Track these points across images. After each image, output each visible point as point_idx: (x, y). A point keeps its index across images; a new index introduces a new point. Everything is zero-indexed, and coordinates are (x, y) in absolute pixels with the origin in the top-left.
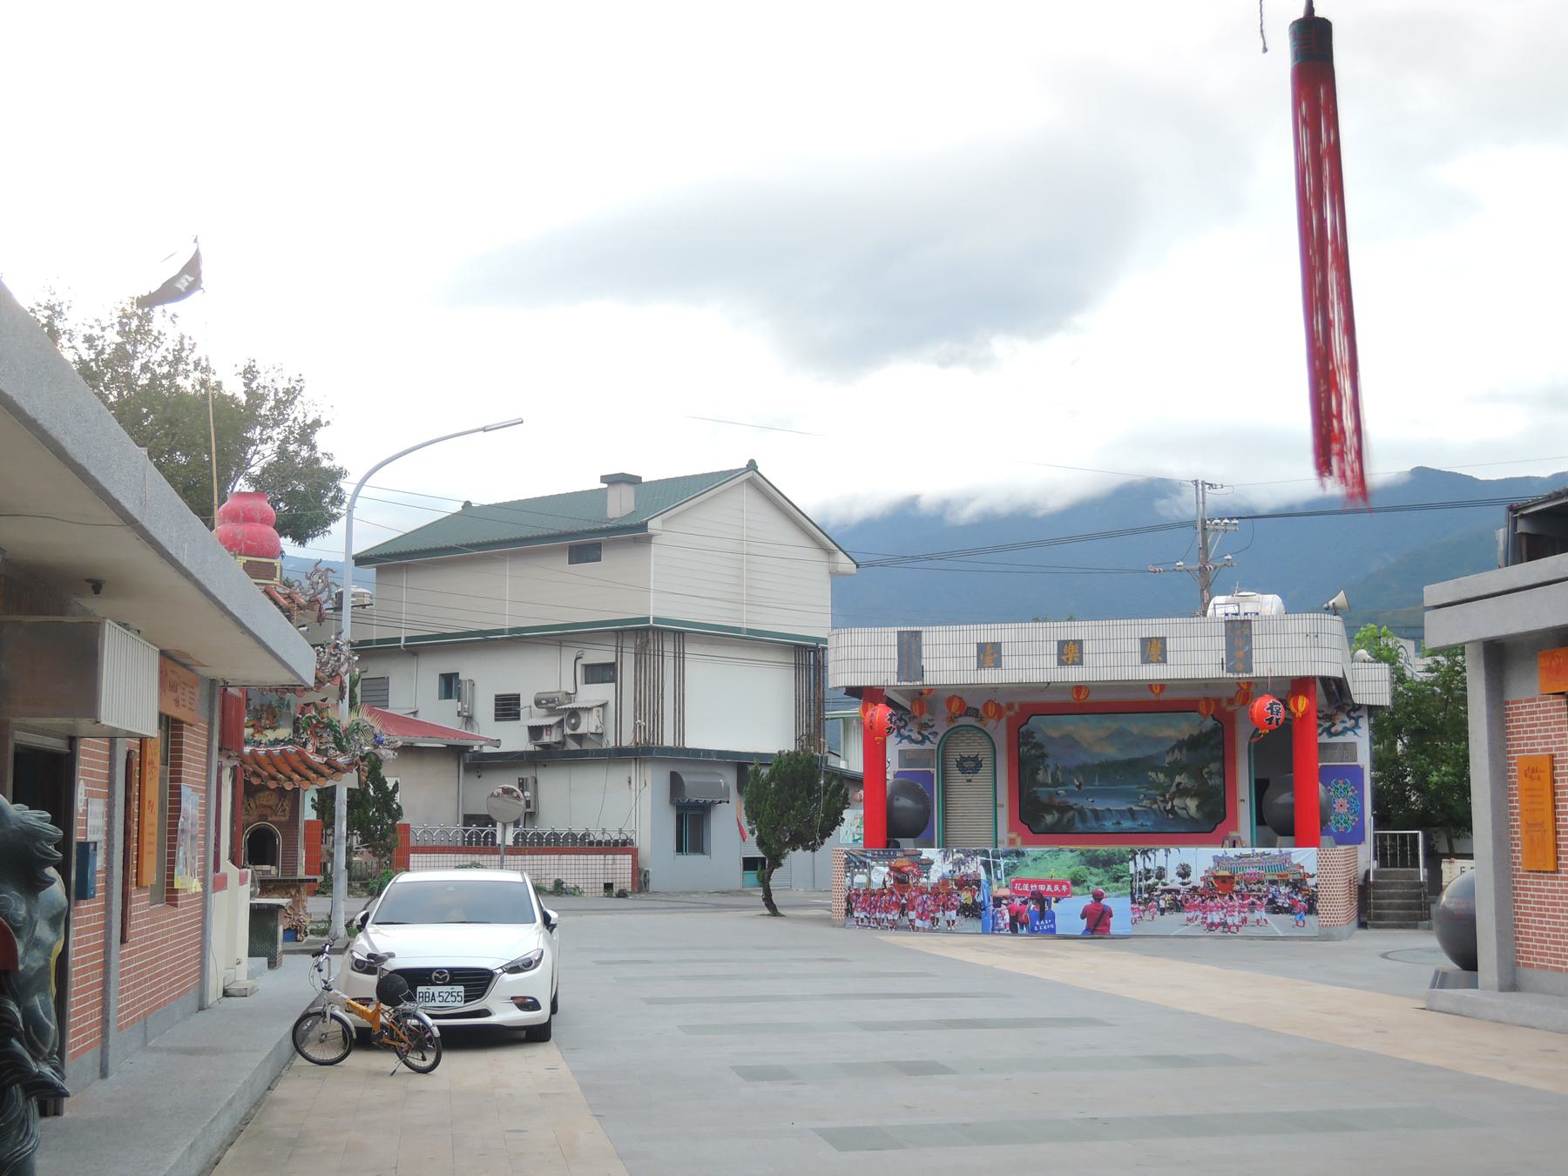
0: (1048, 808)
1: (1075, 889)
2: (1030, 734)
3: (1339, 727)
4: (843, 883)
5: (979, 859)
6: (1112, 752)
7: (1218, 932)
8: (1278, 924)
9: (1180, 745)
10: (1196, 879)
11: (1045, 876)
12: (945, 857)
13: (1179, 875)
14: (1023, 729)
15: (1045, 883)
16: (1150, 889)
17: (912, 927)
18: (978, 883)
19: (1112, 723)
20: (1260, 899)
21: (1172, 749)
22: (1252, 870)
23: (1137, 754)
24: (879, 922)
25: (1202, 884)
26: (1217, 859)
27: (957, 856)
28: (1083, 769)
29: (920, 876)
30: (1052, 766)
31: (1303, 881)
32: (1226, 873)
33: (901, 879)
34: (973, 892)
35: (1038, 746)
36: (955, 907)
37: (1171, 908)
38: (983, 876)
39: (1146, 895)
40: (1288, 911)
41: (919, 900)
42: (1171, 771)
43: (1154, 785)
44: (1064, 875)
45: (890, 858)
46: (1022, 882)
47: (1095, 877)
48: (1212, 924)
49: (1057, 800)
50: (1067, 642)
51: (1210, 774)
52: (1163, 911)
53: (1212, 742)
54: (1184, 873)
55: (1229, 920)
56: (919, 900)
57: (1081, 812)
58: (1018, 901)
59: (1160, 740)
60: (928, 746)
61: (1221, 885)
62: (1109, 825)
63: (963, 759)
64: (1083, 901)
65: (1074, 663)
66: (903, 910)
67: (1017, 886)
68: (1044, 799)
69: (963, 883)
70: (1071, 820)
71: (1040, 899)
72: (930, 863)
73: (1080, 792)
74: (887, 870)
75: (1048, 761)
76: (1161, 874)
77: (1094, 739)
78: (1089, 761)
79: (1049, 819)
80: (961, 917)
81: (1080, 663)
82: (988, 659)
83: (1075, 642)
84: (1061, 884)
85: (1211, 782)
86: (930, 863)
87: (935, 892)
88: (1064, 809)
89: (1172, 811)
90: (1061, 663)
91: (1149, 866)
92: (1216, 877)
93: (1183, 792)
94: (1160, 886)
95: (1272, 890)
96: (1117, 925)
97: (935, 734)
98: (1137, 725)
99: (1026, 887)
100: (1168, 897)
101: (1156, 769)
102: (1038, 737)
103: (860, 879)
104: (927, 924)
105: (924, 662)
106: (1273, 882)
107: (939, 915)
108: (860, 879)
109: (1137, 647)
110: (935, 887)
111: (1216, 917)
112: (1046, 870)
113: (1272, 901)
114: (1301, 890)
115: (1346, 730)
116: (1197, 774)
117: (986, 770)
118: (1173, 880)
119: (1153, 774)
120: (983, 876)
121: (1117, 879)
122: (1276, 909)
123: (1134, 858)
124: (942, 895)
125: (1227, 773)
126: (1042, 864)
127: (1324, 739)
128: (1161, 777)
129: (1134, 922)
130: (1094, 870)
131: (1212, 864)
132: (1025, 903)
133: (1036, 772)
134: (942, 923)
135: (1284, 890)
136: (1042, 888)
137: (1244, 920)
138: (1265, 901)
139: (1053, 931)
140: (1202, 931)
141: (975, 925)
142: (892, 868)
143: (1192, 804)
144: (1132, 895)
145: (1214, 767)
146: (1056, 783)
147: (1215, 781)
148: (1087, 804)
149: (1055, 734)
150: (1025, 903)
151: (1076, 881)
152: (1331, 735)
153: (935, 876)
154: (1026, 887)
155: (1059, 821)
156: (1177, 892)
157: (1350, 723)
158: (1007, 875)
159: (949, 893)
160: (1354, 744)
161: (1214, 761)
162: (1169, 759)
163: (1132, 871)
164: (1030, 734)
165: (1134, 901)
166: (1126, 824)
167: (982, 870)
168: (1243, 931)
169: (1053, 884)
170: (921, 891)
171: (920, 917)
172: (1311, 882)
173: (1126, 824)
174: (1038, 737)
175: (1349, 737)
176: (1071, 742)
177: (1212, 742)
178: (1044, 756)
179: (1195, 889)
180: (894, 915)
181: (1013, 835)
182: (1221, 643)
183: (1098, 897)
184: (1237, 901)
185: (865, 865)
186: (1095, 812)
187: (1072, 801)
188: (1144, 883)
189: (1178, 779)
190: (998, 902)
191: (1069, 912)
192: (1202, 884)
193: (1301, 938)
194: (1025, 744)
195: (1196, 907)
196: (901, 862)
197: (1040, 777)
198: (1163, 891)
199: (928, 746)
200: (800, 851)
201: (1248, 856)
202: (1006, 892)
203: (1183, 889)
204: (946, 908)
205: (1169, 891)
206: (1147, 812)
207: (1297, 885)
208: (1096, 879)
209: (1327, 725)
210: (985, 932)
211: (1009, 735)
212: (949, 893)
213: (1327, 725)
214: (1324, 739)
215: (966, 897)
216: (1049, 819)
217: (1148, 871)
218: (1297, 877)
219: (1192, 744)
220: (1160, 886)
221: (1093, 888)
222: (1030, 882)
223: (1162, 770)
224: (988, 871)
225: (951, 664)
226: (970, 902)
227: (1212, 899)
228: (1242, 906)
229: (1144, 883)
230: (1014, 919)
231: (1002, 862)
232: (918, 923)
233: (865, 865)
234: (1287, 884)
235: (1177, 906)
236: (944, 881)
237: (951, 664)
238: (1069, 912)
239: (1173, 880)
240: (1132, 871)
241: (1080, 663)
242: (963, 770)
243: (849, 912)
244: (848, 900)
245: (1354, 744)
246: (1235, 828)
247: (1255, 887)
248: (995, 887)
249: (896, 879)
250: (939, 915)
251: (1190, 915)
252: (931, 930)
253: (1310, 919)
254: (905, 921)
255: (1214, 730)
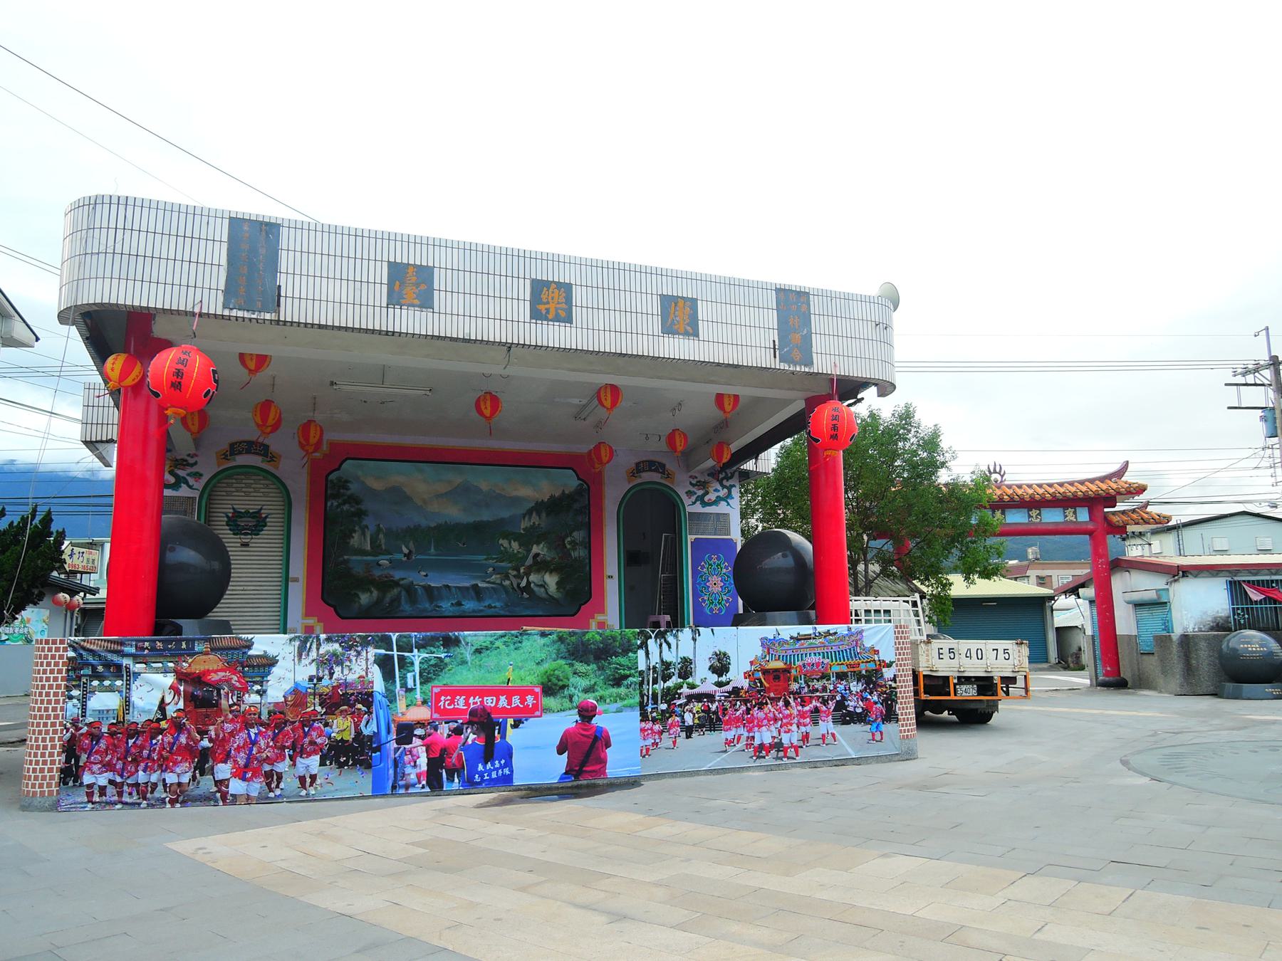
0: (365, 583)
1: (548, 702)
2: (344, 484)
3: (712, 496)
4: (50, 713)
5: (372, 652)
6: (454, 513)
7: (769, 759)
8: (850, 739)
9: (539, 507)
10: (737, 677)
11: (496, 680)
12: (302, 651)
13: (713, 669)
14: (333, 477)
15: (496, 692)
16: (670, 695)
17: (222, 795)
18: (367, 698)
19: (455, 476)
20: (825, 702)
21: (530, 512)
22: (814, 659)
23: (486, 516)
24: (143, 791)
25: (745, 684)
26: (767, 644)
27: (327, 648)
28: (414, 533)
29: (245, 690)
30: (372, 528)
31: (877, 672)
32: (779, 665)
33: (200, 697)
34: (357, 716)
35: (354, 500)
36: (316, 748)
37: (701, 726)
38: (379, 685)
39: (664, 707)
40: (860, 718)
41: (240, 740)
42: (528, 539)
43: (506, 556)
44: (529, 677)
45: (178, 655)
46: (453, 693)
47: (582, 679)
48: (762, 746)
49: (377, 573)
50: (547, 284)
51: (573, 543)
52: (689, 731)
53: (576, 506)
54: (720, 666)
55: (785, 739)
56: (240, 740)
57: (410, 589)
58: (444, 730)
59: (516, 501)
60: (184, 491)
61: (773, 683)
62: (446, 606)
63: (237, 514)
64: (560, 721)
65: (557, 319)
66: (202, 762)
67: (444, 702)
68: (358, 570)
69: (337, 701)
70: (396, 600)
71: (485, 722)
72: (268, 663)
73: (409, 563)
74: (170, 679)
75: (366, 521)
76: (686, 668)
77: (431, 495)
78: (424, 523)
79: (365, 598)
80: (331, 771)
81: (568, 319)
82: (409, 292)
83: (559, 285)
84: (523, 693)
85: (575, 554)
86: (268, 663)
87: (277, 719)
88: (386, 585)
89: (528, 588)
90: (536, 315)
91: (669, 656)
92: (765, 672)
93: (541, 566)
94: (685, 690)
95: (841, 687)
96: (618, 761)
97: (198, 476)
98: (485, 479)
99: (460, 703)
100: (697, 706)
101: (509, 536)
102: (354, 488)
103: (104, 701)
104: (256, 787)
105: (282, 280)
106: (841, 676)
107: (283, 766)
108: (104, 701)
109: (656, 307)
110: (278, 713)
111: (765, 736)
112: (499, 669)
113: (841, 705)
114: (876, 685)
115: (719, 499)
116: (558, 544)
117: (271, 533)
118: (704, 679)
119: (504, 542)
120: (379, 685)
121: (618, 681)
122: (846, 717)
123: (644, 645)
124: (291, 727)
125: (593, 544)
126: (490, 659)
127: (698, 508)
128: (515, 545)
129: (645, 753)
130: (581, 667)
131: (759, 651)
132: (458, 731)
133: (348, 535)
134: (290, 783)
135: (856, 687)
136: (490, 701)
137: (806, 737)
138: (832, 705)
139: (507, 780)
140: (746, 759)
141: (361, 781)
142: (181, 677)
143: (551, 580)
144: (642, 706)
145: (578, 535)
146: (376, 550)
147: (579, 553)
148: (419, 579)
149: (377, 485)
150: (458, 731)
151: (551, 687)
152: (705, 504)
153: (277, 688)
154: (460, 703)
155: (379, 601)
156: (711, 697)
157: (723, 493)
158: (425, 680)
159: (307, 722)
160: (727, 515)
161: (578, 528)
162: (525, 524)
163: (642, 666)
164: (344, 484)
165: (644, 717)
166: (469, 605)
167: (376, 675)
168: (807, 754)
169: (509, 693)
170: (246, 720)
171: (240, 774)
172: (888, 673)
173: (469, 605)
174: (354, 488)
175: (722, 508)
176: (399, 497)
177: (576, 506)
178: (361, 514)
179: (736, 691)
180: (181, 774)
181: (311, 621)
182: (772, 318)
183: (587, 713)
184: (795, 709)
185: (118, 671)
186: (428, 589)
187: (397, 575)
188: (660, 686)
189: (535, 549)
190: (405, 732)
191: (536, 746)
192: (745, 684)
193: (878, 759)
194: (335, 497)
195: (737, 721)
196: (206, 662)
197: (355, 540)
198: (690, 698)
199: (184, 491)
200: (959, 468)
201: (807, 637)
202: (423, 713)
203: (719, 693)
204: (299, 751)
205: (699, 697)
206: (497, 590)
207: (871, 679)
208: (583, 683)
209: (700, 493)
210: (378, 792)
211: (312, 482)
212: (307, 722)
213: (700, 493)
214: (698, 508)
215: (341, 727)
216: (365, 598)
217: (667, 665)
218: (871, 666)
219: (553, 506)
220: (685, 690)
221: (580, 697)
222: (468, 692)
223: (517, 537)
224: (388, 675)
225: (338, 291)
226: (349, 736)
227: (761, 706)
228: (802, 715)
229: (660, 686)
230: (435, 765)
231: (417, 657)
232: (236, 786)
233: (118, 671)
234: (859, 677)
235: (710, 722)
236: (298, 697)
237: (338, 291)
238: (536, 746)
239: (704, 679)
240: (642, 666)
241: (568, 319)
242: (237, 530)
243: (70, 774)
244: (70, 749)
245: (727, 515)
246: (602, 610)
247: (818, 685)
248: (401, 705)
249: (190, 698)
250: (283, 766)
251: (730, 735)
252: (263, 800)
253: (888, 728)
254: (207, 784)
255: (579, 492)
